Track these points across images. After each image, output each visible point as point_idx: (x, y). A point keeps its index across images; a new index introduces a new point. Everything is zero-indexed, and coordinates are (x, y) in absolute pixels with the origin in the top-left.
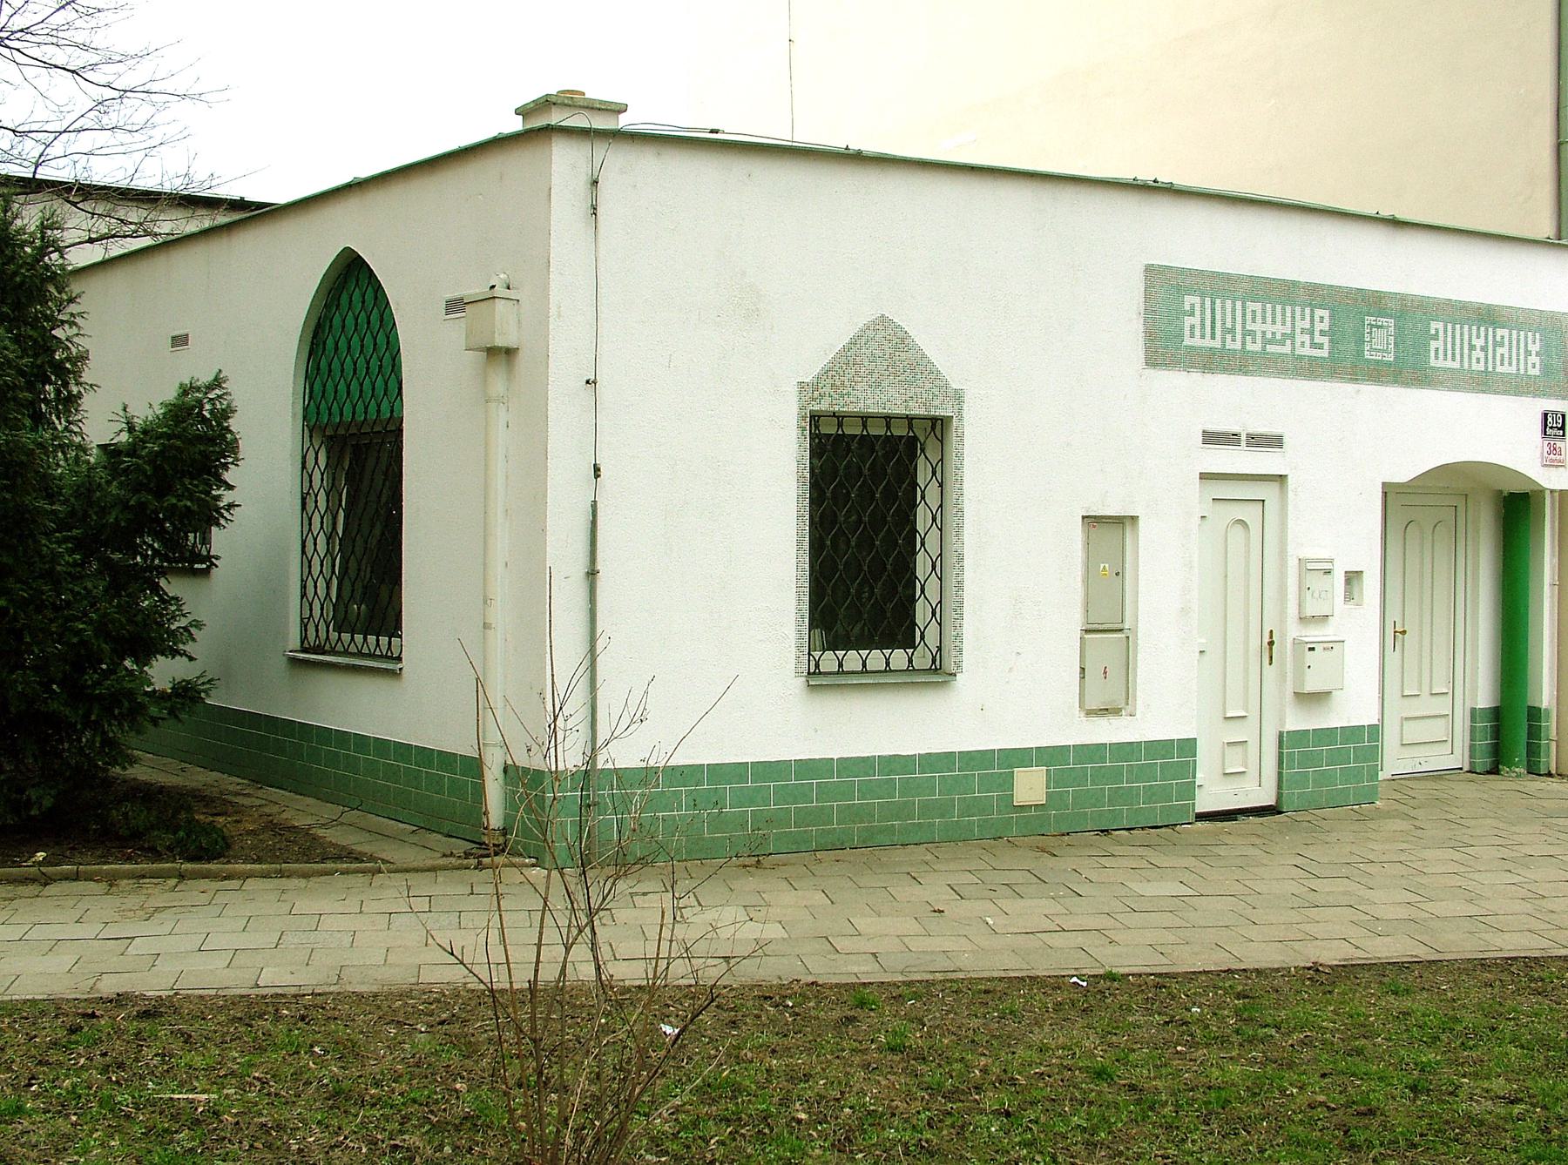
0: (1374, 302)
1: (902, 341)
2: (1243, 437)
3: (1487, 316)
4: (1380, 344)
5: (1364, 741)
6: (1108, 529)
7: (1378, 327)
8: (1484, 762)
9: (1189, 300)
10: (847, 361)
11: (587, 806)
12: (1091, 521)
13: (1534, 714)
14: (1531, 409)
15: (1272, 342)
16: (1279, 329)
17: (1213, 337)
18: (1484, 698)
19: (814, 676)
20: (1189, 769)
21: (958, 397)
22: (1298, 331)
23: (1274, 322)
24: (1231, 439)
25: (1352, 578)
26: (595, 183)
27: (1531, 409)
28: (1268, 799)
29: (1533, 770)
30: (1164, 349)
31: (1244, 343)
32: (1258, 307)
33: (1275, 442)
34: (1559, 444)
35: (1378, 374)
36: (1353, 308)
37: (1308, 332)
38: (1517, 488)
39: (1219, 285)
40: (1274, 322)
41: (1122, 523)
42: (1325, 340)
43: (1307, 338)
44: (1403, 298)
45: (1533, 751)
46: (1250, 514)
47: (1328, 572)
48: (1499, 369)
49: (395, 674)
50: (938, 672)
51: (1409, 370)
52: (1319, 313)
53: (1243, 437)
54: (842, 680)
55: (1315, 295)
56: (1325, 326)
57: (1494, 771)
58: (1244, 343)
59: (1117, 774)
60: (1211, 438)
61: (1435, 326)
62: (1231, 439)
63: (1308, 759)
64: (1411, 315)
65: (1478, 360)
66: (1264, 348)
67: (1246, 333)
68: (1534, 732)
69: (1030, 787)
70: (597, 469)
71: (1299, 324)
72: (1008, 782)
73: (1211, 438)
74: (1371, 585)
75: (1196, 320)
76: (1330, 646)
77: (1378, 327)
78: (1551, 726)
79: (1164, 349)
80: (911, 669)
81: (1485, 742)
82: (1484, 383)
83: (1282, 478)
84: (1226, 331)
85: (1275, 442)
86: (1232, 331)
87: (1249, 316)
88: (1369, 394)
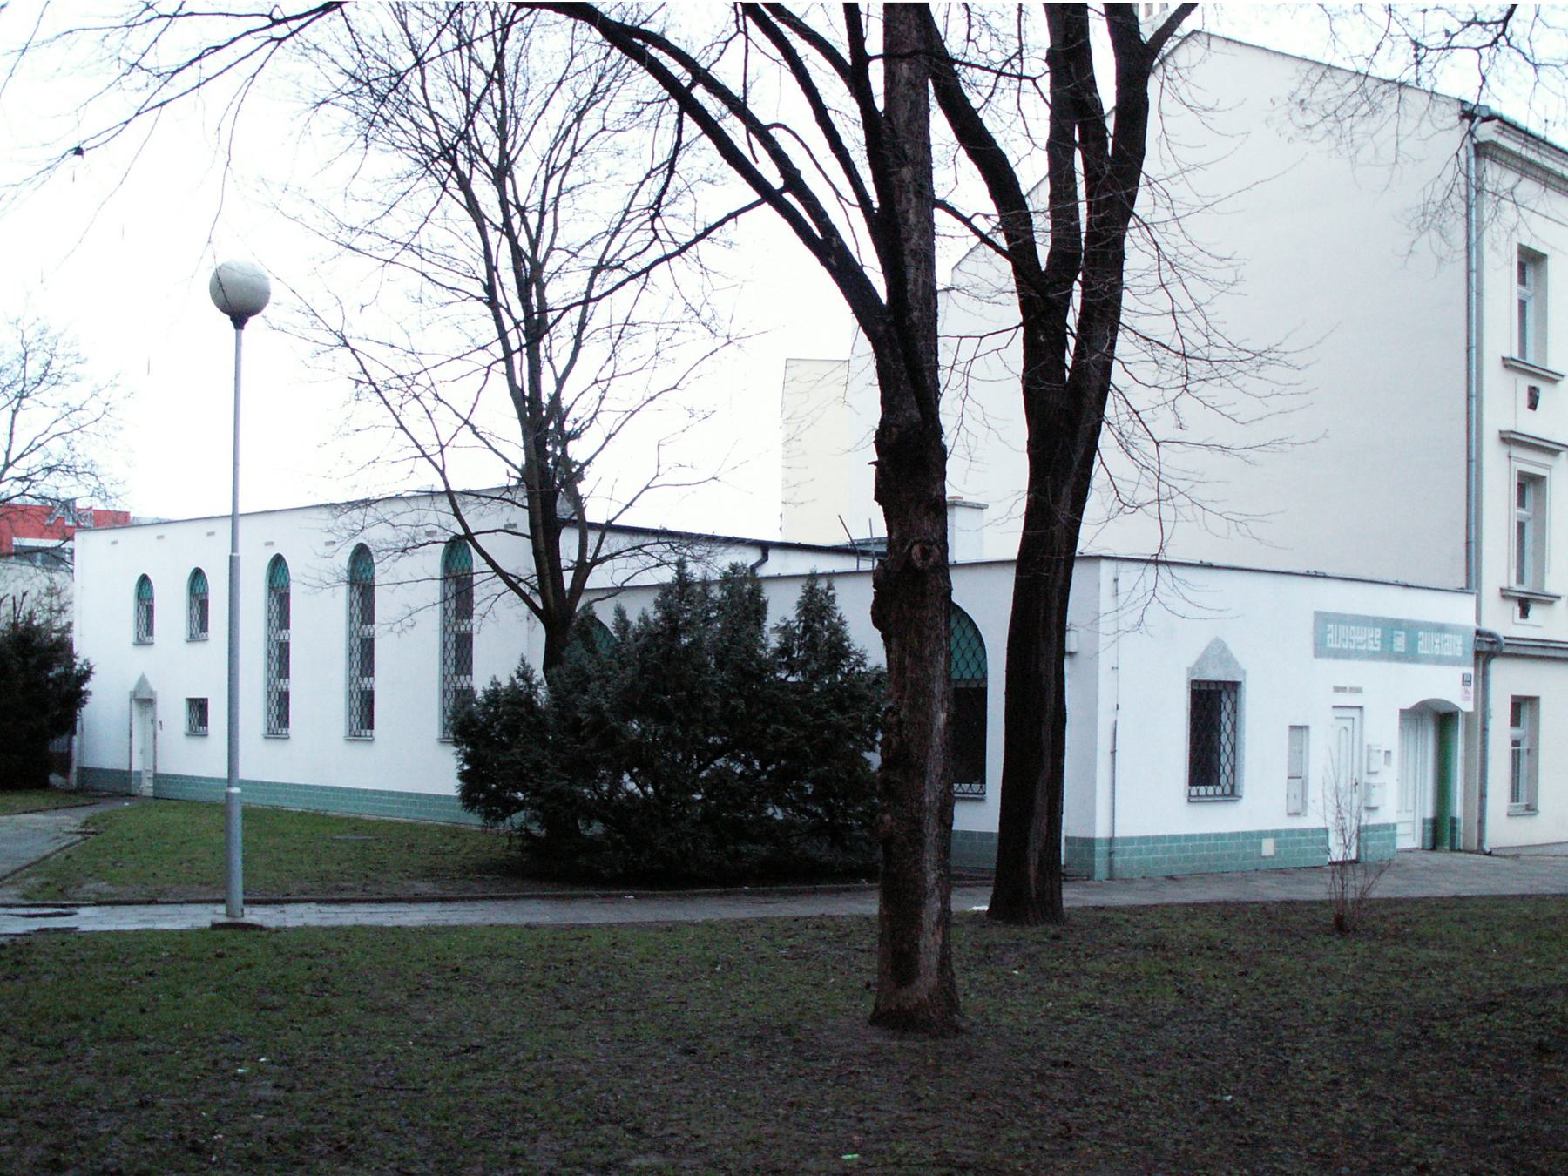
0: (1396, 624)
1: (1224, 649)
3: (1441, 628)
4: (1400, 644)
5: (1390, 828)
6: (1299, 729)
8: (1428, 845)
9: (1330, 626)
10: (1204, 658)
11: (1111, 853)
12: (1292, 727)
13: (1454, 821)
18: (1429, 815)
19: (1191, 799)
20: (1325, 842)
21: (1244, 673)
24: (1343, 689)
25: (1388, 752)
26: (1116, 580)
29: (1453, 849)
30: (1321, 650)
33: (1358, 690)
35: (1398, 657)
36: (1391, 627)
37: (1370, 638)
38: (1447, 710)
39: (1341, 619)
41: (1304, 728)
44: (1409, 622)
45: (1453, 840)
46: (1348, 724)
49: (982, 800)
50: (1233, 795)
51: (1411, 656)
55: (1375, 622)
57: (1434, 849)
59: (1299, 843)
60: (1337, 689)
61: (1421, 634)
62: (1343, 689)
64: (1411, 629)
68: (1453, 829)
69: (1268, 847)
73: (1337, 689)
74: (1395, 755)
76: (1380, 786)
78: (1461, 826)
79: (1321, 650)
80: (1224, 795)
81: (1429, 835)
82: (1438, 660)
83: (1361, 708)
85: (1358, 690)
88: (1396, 666)
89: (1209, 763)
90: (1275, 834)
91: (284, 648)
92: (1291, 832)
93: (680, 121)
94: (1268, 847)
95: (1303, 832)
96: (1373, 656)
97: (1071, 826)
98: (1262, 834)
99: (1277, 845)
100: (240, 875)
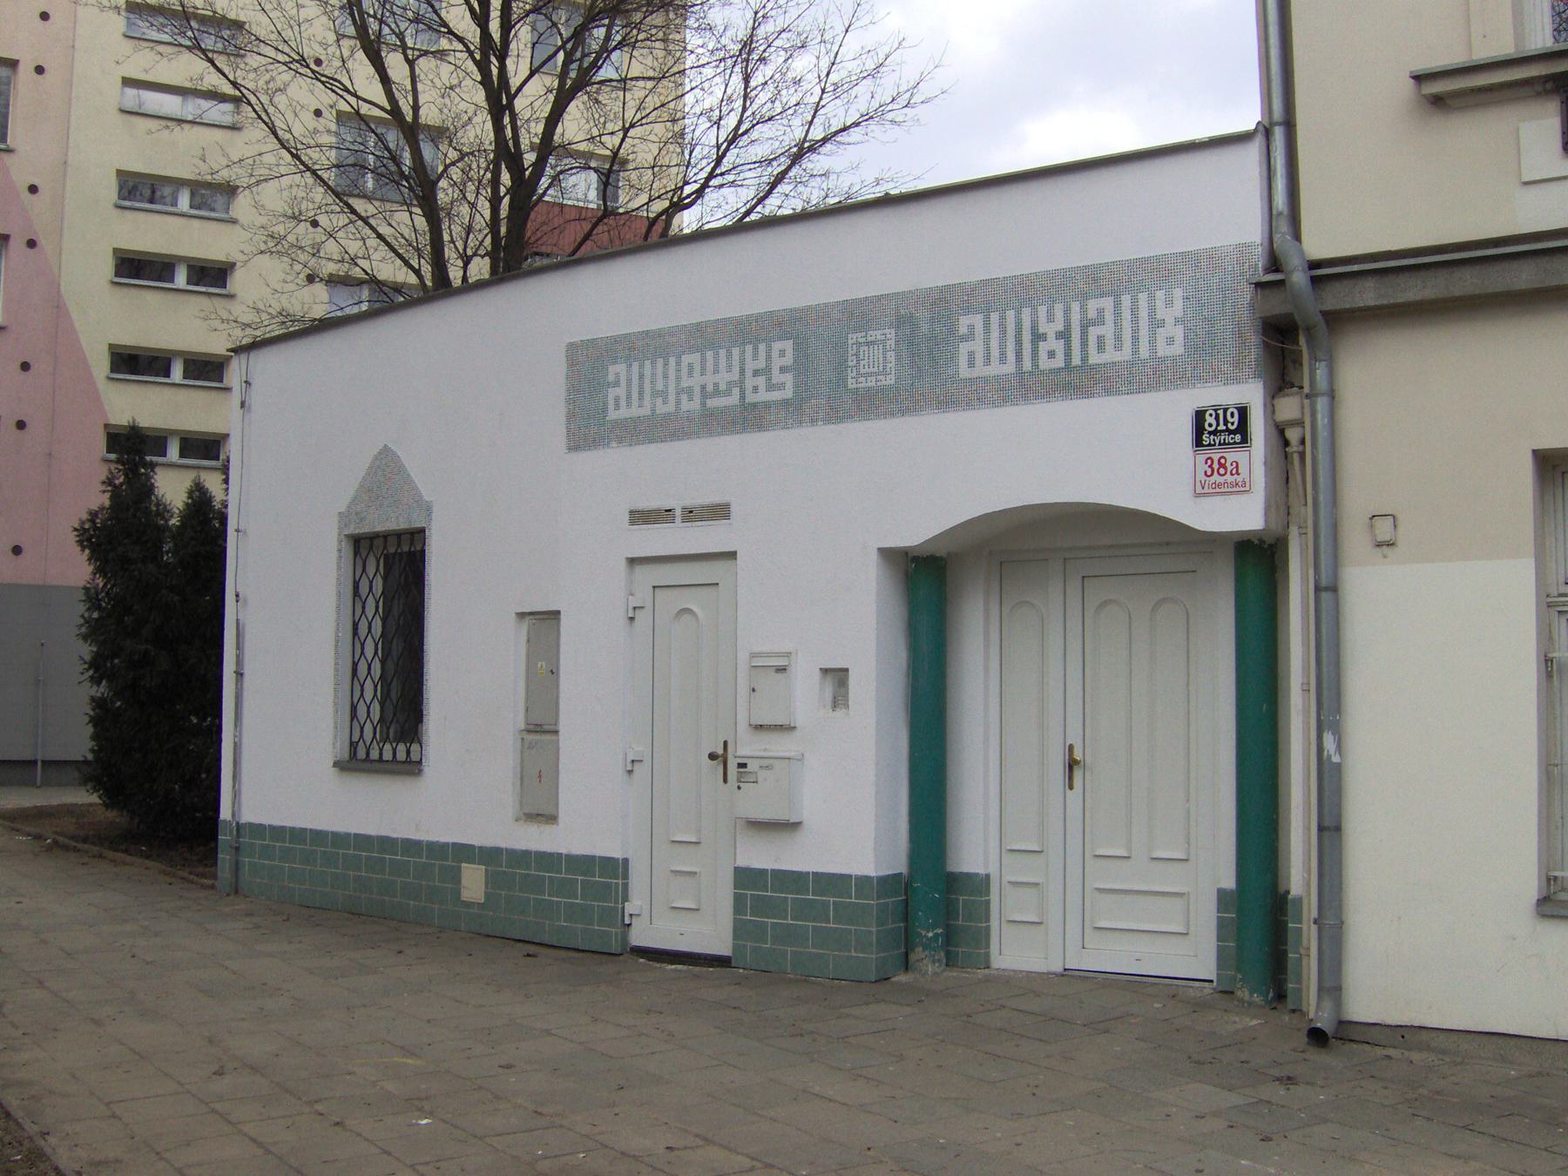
7: (868, 344)
17: (1003, 359)
21: (429, 510)
24: (661, 516)
33: (720, 512)
35: (870, 404)
60: (641, 517)
62: (661, 516)
73: (641, 517)
85: (720, 512)
89: (391, 709)
90: (488, 856)
91: (238, 648)
92: (521, 858)
93: (520, 89)
94: (473, 883)
95: (548, 860)
96: (795, 411)
97: (225, 813)
98: (464, 852)
99: (492, 880)
100: (55, 802)
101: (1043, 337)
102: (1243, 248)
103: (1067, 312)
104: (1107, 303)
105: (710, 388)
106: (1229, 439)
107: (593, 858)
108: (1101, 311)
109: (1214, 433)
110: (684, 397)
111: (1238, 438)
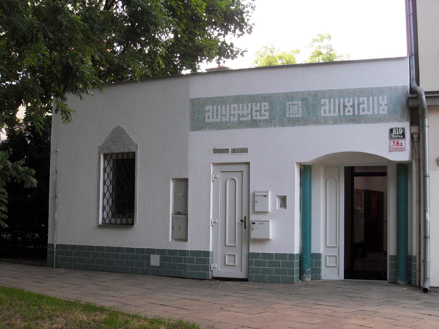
2: (230, 150)
7: (293, 105)
14: (386, 127)
15: (243, 116)
16: (245, 112)
17: (334, 112)
20: (207, 261)
21: (137, 147)
22: (254, 111)
23: (243, 110)
27: (386, 127)
28: (242, 275)
31: (230, 118)
32: (236, 105)
33: (245, 150)
34: (400, 141)
40: (243, 110)
42: (267, 113)
43: (258, 114)
47: (266, 196)
48: (361, 113)
52: (263, 104)
53: (230, 150)
54: (110, 225)
56: (267, 108)
58: (230, 118)
60: (216, 151)
63: (258, 263)
65: (349, 111)
66: (239, 119)
67: (230, 115)
70: (56, 171)
71: (254, 109)
72: (149, 259)
73: (216, 151)
75: (210, 114)
77: (293, 105)
84: (222, 115)
85: (245, 150)
86: (225, 115)
87: (232, 109)
101: (347, 107)
102: (404, 87)
103: (354, 100)
104: (365, 99)
105: (241, 115)
106: (400, 137)
107: (200, 251)
108: (363, 101)
109: (396, 135)
110: (232, 117)
111: (402, 136)
